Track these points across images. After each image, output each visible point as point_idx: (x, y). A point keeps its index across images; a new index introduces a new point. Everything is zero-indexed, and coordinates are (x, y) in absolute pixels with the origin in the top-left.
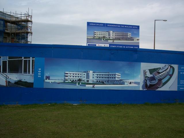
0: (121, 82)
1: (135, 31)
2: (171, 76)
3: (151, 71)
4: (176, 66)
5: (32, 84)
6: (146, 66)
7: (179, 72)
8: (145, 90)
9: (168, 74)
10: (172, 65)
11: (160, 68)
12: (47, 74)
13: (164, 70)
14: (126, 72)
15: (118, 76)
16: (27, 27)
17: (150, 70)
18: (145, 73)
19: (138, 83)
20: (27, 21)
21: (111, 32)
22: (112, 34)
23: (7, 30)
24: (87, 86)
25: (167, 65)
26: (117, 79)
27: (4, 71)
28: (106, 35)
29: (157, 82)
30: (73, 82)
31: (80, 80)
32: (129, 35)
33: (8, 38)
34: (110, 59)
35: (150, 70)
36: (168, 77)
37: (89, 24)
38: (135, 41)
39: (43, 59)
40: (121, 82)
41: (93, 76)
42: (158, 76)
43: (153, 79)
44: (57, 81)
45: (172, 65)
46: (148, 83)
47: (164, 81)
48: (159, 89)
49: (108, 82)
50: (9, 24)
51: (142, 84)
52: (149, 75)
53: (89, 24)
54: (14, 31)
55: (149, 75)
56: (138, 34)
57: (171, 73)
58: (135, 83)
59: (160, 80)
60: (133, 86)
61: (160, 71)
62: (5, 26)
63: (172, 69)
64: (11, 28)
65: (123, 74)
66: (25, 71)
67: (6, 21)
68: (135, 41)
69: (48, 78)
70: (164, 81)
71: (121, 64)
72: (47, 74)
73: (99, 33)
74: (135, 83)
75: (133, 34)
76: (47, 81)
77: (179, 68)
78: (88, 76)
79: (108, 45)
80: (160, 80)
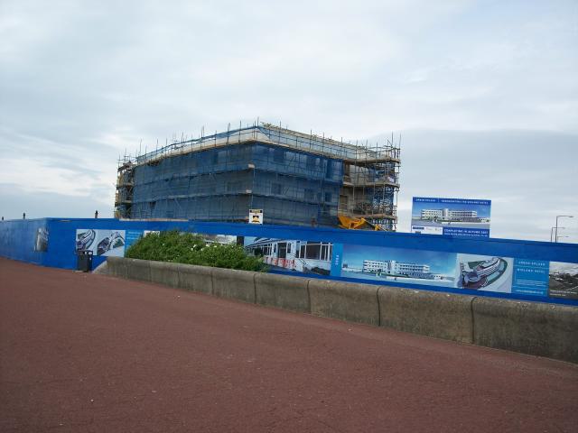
0: (429, 276)
1: (484, 209)
2: (502, 272)
3: (471, 265)
4: (510, 261)
5: (329, 271)
6: (463, 259)
7: (515, 269)
8: (195, 234)
9: (497, 270)
10: (504, 258)
11: (485, 261)
12: (344, 262)
13: (490, 264)
14: (438, 264)
15: (426, 269)
16: (392, 174)
17: (469, 263)
18: (462, 266)
19: (452, 279)
20: (392, 162)
21: (447, 210)
22: (448, 213)
23: (349, 180)
24: (388, 277)
25: (496, 259)
26: (424, 272)
27: (302, 256)
28: (439, 214)
29: (479, 279)
30: (372, 273)
31: (380, 270)
32: (474, 214)
33: (349, 198)
34: (417, 249)
35: (469, 263)
36: (498, 273)
37: (415, 200)
38: (483, 222)
39: (341, 246)
40: (429, 276)
41: (395, 267)
42: (481, 272)
43: (473, 274)
44: (355, 270)
45: (504, 258)
46: (467, 280)
47: (489, 279)
48: (482, 289)
49: (413, 275)
50: (352, 167)
51: (457, 280)
52: (467, 269)
53: (415, 200)
54: (362, 182)
55: (467, 269)
56: (488, 213)
57: (501, 269)
58: (448, 278)
59: (484, 277)
60: (445, 282)
61: (485, 265)
62: (345, 172)
63: (503, 263)
64: (358, 177)
65: (433, 266)
66: (323, 258)
67: (348, 163)
68: (483, 222)
69: (345, 266)
70: (489, 279)
71: (430, 253)
72: (344, 262)
73: (429, 212)
74: (448, 278)
75: (480, 212)
76: (345, 269)
77: (515, 263)
78: (389, 267)
79: (439, 231)
80: (484, 277)
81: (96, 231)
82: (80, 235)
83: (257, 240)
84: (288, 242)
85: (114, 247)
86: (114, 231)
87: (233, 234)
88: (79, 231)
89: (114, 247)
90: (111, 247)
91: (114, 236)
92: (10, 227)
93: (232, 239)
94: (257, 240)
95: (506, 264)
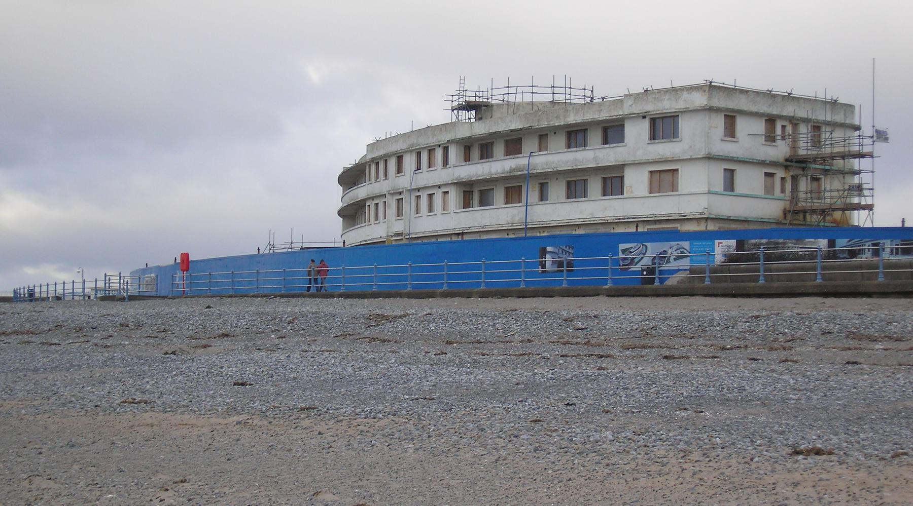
11: (632, 248)
25: (639, 245)
29: (629, 262)
57: (644, 252)
61: (632, 251)
63: (644, 247)
80: (633, 259)
81: (648, 244)
82: (624, 251)
83: (849, 241)
84: (882, 242)
85: (675, 259)
86: (673, 243)
87: (824, 238)
88: (622, 246)
89: (675, 259)
90: (672, 259)
91: (674, 248)
92: (798, 179)
93: (438, 240)
94: (849, 241)
95: (646, 247)
